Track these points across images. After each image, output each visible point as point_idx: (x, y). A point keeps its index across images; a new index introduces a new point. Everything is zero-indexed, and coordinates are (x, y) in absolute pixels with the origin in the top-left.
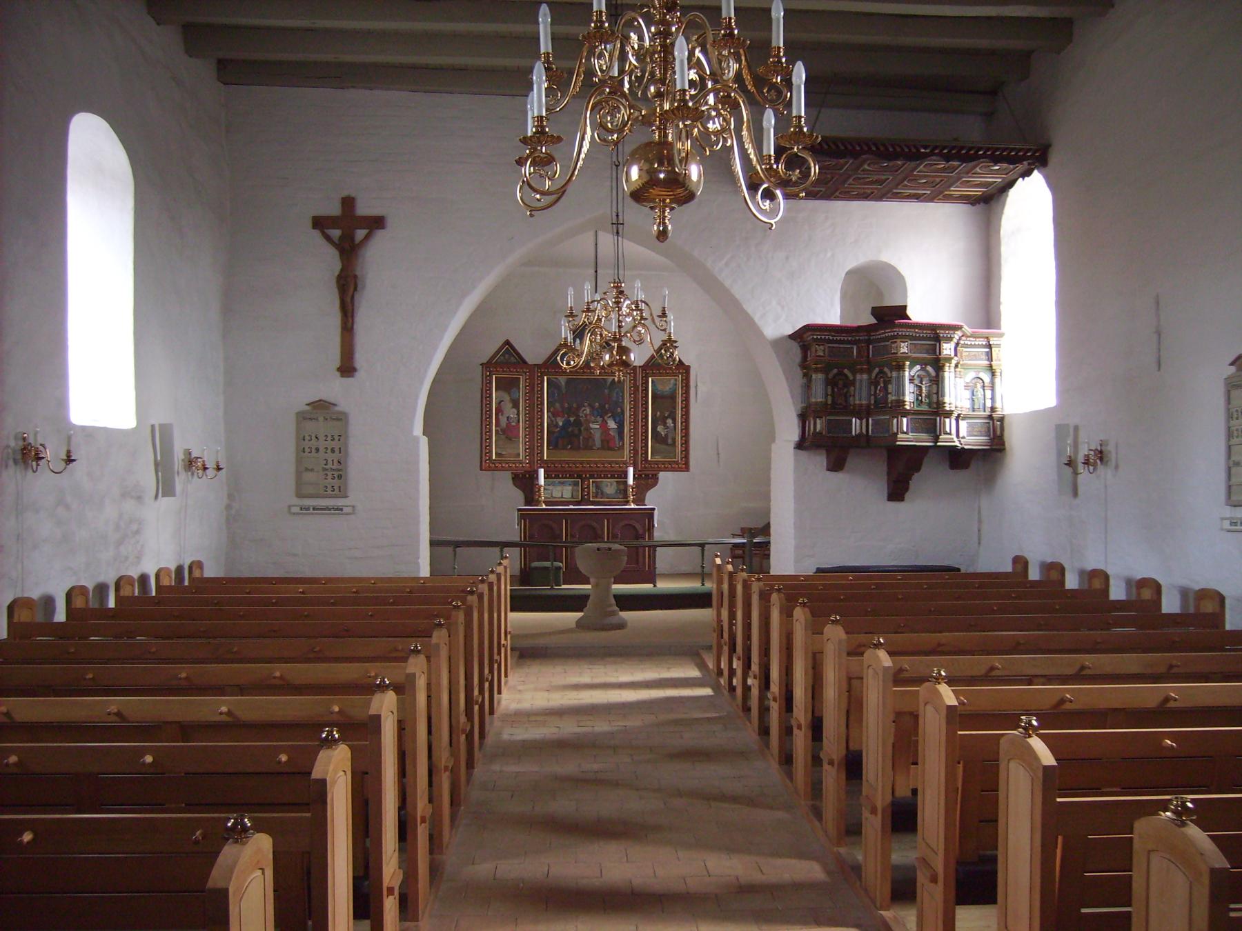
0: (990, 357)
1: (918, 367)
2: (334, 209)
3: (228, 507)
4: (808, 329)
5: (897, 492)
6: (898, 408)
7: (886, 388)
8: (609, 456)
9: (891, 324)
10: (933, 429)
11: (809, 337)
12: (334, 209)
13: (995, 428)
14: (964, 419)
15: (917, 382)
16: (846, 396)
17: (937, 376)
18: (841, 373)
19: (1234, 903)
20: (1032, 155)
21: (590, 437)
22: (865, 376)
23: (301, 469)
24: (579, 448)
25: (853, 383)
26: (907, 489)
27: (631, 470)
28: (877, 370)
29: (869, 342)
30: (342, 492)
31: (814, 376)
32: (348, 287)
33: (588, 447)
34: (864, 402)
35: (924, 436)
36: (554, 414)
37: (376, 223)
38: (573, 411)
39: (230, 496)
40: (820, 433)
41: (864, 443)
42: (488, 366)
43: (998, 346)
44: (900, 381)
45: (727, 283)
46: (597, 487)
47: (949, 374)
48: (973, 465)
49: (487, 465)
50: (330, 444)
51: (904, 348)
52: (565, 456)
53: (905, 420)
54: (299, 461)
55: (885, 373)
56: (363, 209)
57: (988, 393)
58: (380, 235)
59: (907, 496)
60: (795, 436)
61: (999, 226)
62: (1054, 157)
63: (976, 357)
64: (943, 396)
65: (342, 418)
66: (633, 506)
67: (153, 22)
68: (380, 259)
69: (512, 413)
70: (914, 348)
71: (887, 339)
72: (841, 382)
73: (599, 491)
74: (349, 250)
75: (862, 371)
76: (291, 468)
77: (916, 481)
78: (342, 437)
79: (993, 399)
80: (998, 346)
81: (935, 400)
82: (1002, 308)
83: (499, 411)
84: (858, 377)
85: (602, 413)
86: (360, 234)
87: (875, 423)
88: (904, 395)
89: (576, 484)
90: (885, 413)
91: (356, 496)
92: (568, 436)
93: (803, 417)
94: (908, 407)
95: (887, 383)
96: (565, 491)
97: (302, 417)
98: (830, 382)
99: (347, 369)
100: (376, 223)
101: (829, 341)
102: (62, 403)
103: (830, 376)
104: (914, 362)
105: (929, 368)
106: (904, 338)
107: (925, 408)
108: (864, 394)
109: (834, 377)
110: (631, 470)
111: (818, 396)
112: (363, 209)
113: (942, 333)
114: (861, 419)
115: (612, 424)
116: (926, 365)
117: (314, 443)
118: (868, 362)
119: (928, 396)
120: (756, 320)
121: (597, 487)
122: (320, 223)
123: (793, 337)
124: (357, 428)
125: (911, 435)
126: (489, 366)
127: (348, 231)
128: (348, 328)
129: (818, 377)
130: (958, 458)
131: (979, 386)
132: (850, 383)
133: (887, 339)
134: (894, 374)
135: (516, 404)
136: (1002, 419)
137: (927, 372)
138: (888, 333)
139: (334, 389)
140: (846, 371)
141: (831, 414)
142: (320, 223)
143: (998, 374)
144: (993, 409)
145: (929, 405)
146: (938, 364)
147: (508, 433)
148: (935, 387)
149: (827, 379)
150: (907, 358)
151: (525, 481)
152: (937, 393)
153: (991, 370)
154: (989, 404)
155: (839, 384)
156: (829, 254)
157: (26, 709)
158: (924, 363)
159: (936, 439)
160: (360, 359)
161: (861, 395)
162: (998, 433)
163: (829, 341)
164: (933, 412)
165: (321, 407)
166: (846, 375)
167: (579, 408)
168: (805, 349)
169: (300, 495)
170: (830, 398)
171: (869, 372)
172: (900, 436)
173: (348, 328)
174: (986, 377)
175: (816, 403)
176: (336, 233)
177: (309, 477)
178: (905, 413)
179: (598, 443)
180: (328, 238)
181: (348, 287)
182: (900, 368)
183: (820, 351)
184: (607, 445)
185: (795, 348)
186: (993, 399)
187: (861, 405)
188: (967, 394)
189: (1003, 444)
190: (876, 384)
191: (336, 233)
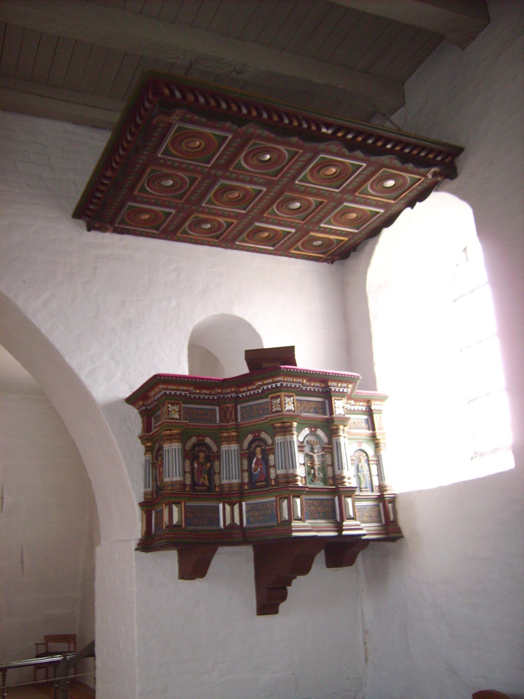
1: (306, 431)
4: (158, 380)
5: (270, 600)
6: (287, 486)
7: (265, 460)
9: (275, 372)
11: (156, 394)
13: (386, 507)
15: (307, 450)
16: (211, 473)
17: (330, 442)
18: (201, 444)
20: (437, 164)
22: (234, 447)
25: (218, 457)
26: (283, 597)
28: (250, 437)
29: (237, 400)
31: (166, 446)
34: (235, 481)
35: (322, 523)
40: (178, 526)
41: (234, 536)
43: (380, 412)
45: (44, 329)
48: (360, 558)
51: (289, 405)
53: (298, 501)
55: (263, 441)
57: (374, 469)
59: (282, 606)
60: (137, 531)
62: (467, 165)
64: (341, 468)
71: (264, 394)
72: (202, 455)
75: (229, 440)
77: (299, 588)
79: (380, 475)
80: (380, 412)
81: (330, 474)
82: (376, 369)
84: (225, 447)
87: (251, 509)
88: (294, 467)
90: (268, 493)
93: (148, 506)
94: (300, 484)
95: (265, 454)
98: (190, 455)
101: (188, 400)
103: (188, 446)
105: (320, 432)
107: (319, 484)
108: (235, 469)
109: (194, 446)
111: (174, 472)
113: (334, 386)
114: (232, 505)
116: (316, 428)
118: (237, 427)
119: (323, 468)
120: (83, 375)
123: (131, 400)
125: (308, 523)
129: (172, 450)
130: (342, 551)
131: (363, 459)
132: (213, 457)
133: (264, 394)
134: (279, 439)
136: (393, 500)
137: (318, 437)
138: (268, 384)
140: (208, 440)
141: (192, 497)
144: (382, 488)
145: (325, 480)
146: (330, 426)
148: (328, 457)
149: (184, 450)
150: (294, 417)
152: (332, 465)
153: (374, 439)
154: (376, 483)
155: (201, 457)
156: (174, 303)
158: (313, 426)
159: (339, 527)
161: (230, 471)
162: (392, 518)
163: (188, 400)
164: (332, 492)
166: (207, 446)
168: (148, 416)
170: (188, 476)
171: (239, 440)
172: (295, 524)
174: (370, 449)
175: (173, 484)
178: (298, 492)
182: (287, 430)
183: (174, 412)
185: (134, 419)
186: (380, 475)
187: (230, 485)
189: (398, 531)
190: (250, 455)
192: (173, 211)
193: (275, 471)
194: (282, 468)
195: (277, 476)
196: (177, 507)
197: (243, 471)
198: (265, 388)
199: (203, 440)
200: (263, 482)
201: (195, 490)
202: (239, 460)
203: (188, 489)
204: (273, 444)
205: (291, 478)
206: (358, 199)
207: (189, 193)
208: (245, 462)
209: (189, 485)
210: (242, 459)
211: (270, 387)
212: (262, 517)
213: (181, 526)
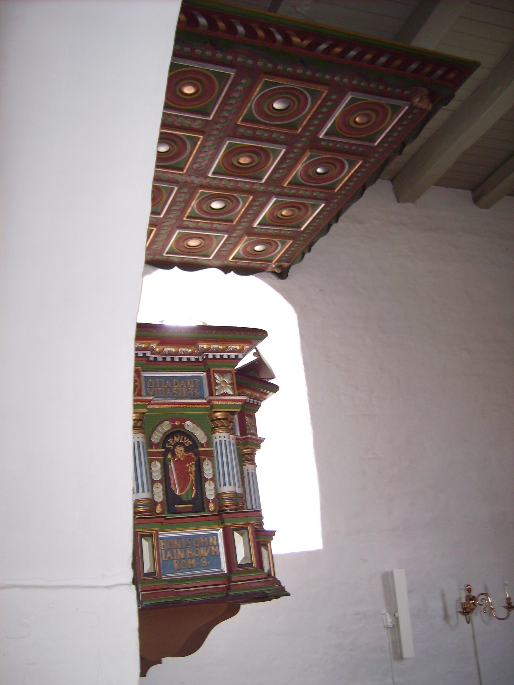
18: (178, 431)
72: (180, 451)
140: (189, 425)
141: (167, 523)
166: (190, 436)
192: (232, 73)
193: (216, 488)
194: (230, 485)
195: (219, 496)
196: (242, 535)
197: (153, 482)
198: (210, 355)
199: (182, 426)
200: (189, 503)
201: (172, 511)
202: (238, 467)
203: (159, 509)
204: (209, 443)
206: (241, 130)
207: (309, 117)
208: (157, 466)
209: (161, 503)
210: (150, 462)
211: (218, 355)
212: (193, 561)
213: (251, 565)
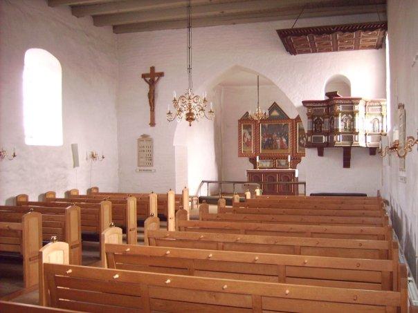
0: (381, 110)
2: (148, 71)
3: (119, 170)
8: (282, 151)
10: (351, 139)
12: (148, 71)
14: (369, 135)
16: (321, 127)
18: (318, 119)
19: (68, 290)
21: (276, 146)
23: (139, 157)
24: (272, 149)
27: (289, 157)
30: (151, 165)
32: (152, 97)
33: (276, 148)
35: (347, 142)
36: (264, 137)
37: (161, 74)
38: (271, 136)
39: (119, 166)
42: (240, 121)
44: (337, 121)
46: (279, 162)
47: (358, 119)
49: (241, 155)
50: (143, 149)
52: (268, 152)
54: (139, 155)
56: (157, 71)
58: (162, 78)
61: (21, 80)
63: (375, 110)
65: (151, 140)
66: (290, 169)
67: (76, 18)
68: (161, 85)
69: (248, 137)
70: (343, 108)
73: (280, 164)
74: (152, 84)
76: (136, 157)
78: (151, 147)
83: (244, 136)
85: (281, 136)
86: (156, 78)
89: (271, 162)
91: (156, 166)
92: (269, 145)
96: (267, 164)
97: (139, 140)
99: (153, 124)
100: (161, 74)
102: (21, 137)
104: (343, 113)
105: (350, 115)
106: (339, 104)
107: (348, 131)
110: (289, 157)
112: (157, 71)
115: (284, 140)
117: (143, 149)
119: (350, 126)
120: (291, 99)
121: (279, 162)
122: (144, 76)
124: (156, 144)
126: (240, 121)
127: (152, 78)
128: (152, 110)
131: (377, 122)
132: (321, 123)
135: (250, 134)
139: (149, 131)
142: (144, 76)
143: (385, 117)
146: (353, 114)
147: (248, 144)
151: (253, 160)
154: (380, 129)
156: (319, 74)
157: (5, 225)
158: (347, 114)
160: (157, 121)
161: (326, 128)
164: (351, 132)
165: (144, 136)
167: (326, 118)
169: (139, 166)
173: (152, 110)
174: (380, 118)
176: (148, 79)
177: (141, 160)
178: (339, 134)
179: (279, 146)
180: (146, 81)
181: (152, 97)
182: (337, 116)
184: (282, 147)
188: (372, 125)
191: (148, 79)
205: (337, 130)
